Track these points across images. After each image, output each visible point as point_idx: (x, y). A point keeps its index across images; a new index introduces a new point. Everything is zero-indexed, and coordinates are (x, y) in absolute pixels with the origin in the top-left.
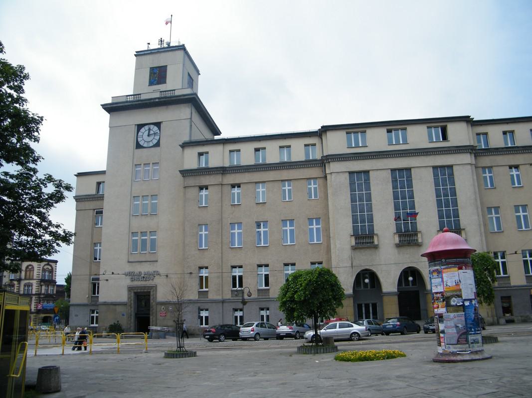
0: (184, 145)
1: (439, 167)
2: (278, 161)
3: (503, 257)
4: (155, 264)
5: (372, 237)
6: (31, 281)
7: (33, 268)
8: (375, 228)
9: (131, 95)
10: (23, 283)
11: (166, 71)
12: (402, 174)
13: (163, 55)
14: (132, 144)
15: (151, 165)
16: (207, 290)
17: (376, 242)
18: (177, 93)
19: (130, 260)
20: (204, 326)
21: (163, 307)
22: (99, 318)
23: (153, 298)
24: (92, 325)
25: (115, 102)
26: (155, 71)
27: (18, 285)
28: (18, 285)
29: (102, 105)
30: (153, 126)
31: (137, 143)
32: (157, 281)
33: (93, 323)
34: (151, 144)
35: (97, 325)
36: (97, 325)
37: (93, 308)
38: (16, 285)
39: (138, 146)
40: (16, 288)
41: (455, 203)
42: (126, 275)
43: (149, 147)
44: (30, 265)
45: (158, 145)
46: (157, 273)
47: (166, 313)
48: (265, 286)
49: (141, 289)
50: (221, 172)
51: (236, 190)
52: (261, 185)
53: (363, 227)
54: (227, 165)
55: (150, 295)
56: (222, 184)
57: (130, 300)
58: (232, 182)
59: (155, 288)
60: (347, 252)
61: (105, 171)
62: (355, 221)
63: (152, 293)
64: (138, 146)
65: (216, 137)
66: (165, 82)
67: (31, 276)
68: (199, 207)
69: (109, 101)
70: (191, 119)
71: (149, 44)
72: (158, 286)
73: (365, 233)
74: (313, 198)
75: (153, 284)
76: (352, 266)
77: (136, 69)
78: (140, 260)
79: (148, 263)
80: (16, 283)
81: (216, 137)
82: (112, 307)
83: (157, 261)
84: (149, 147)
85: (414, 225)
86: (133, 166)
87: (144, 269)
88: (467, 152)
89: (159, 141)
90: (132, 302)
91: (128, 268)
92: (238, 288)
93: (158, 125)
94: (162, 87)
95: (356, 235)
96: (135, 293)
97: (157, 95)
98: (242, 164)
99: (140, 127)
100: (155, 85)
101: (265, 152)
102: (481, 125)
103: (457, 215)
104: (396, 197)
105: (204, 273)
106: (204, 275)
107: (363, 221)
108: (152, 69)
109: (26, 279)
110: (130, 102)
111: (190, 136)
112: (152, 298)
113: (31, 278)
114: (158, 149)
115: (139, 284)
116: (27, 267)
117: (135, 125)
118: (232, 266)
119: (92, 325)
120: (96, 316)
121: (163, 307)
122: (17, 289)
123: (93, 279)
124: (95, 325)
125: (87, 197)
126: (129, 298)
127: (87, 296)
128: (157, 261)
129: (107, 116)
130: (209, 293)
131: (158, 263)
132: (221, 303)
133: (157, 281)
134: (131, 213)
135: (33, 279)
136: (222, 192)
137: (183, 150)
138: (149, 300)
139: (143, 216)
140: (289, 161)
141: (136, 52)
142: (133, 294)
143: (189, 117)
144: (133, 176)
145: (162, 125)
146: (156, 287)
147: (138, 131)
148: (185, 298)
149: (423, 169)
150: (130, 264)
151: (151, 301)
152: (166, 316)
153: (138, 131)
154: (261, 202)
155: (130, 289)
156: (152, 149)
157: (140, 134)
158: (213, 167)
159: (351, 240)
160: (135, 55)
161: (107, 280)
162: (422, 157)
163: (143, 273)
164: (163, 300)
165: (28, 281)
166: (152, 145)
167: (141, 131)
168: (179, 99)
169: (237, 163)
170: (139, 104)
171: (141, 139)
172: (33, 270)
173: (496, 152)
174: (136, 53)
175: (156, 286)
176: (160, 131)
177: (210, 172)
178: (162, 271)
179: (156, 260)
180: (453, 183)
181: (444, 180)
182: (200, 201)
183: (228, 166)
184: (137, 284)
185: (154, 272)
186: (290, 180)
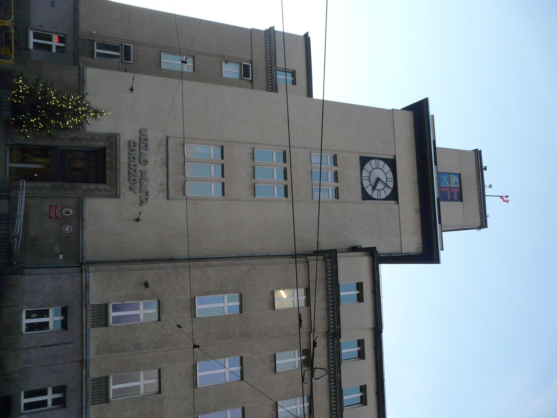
1: (106, 321)
2: (341, 282)
4: (163, 195)
15: (336, 185)
19: (170, 141)
20: (25, 321)
21: (71, 212)
24: (31, 34)
30: (392, 187)
33: (36, 36)
35: (31, 46)
36: (31, 46)
37: (69, 40)
42: (142, 133)
43: (362, 180)
45: (366, 197)
47: (57, 217)
48: (27, 324)
50: (332, 330)
57: (88, 137)
63: (101, 186)
64: (364, 160)
78: (170, 162)
79: (165, 180)
83: (168, 198)
84: (362, 180)
86: (335, 150)
88: (329, 327)
90: (84, 143)
93: (394, 196)
96: (103, 150)
98: (338, 258)
99: (392, 163)
112: (92, 186)
117: (395, 156)
119: (31, 34)
120: (51, 46)
121: (71, 212)
123: (127, 49)
124: (32, 41)
126: (93, 136)
127: (94, 33)
128: (168, 198)
132: (80, 359)
138: (86, 180)
139: (252, 169)
140: (343, 357)
142: (100, 144)
145: (393, 202)
146: (116, 196)
147: (385, 160)
148: (91, 275)
151: (85, 186)
152: (51, 217)
153: (385, 160)
157: (381, 163)
161: (132, 90)
163: (146, 168)
164: (86, 212)
166: (365, 186)
167: (386, 165)
169: (344, 353)
173: (332, 291)
175: (119, 197)
177: (335, 396)
178: (147, 209)
179: (171, 196)
184: (122, 155)
185: (147, 193)
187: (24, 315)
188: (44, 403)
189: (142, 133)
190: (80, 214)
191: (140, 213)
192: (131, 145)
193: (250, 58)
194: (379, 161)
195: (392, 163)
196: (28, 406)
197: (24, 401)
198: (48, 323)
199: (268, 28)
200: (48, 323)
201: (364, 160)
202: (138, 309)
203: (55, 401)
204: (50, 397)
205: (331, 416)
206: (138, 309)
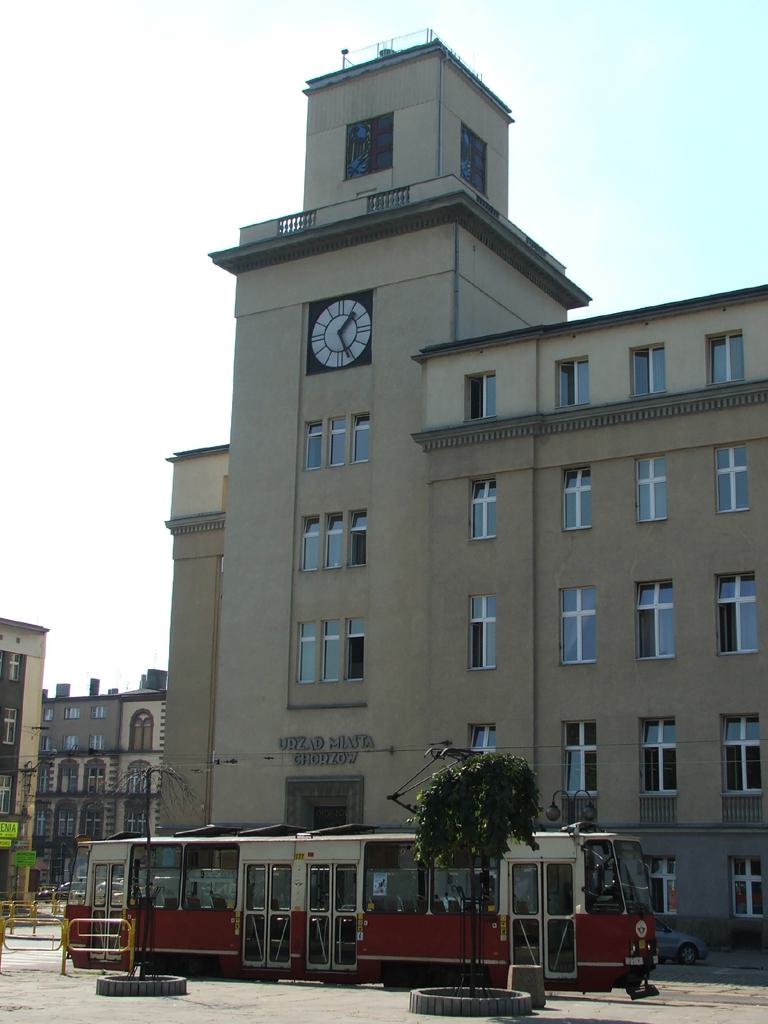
0: (427, 355)
3: (591, 739)
6: (145, 758)
7: (151, 719)
9: (296, 216)
10: (126, 761)
11: (390, 130)
14: (296, 362)
16: (755, 791)
18: (415, 196)
19: (296, 702)
22: (763, 887)
25: (251, 240)
26: (362, 133)
27: (113, 769)
28: (113, 769)
29: (211, 255)
30: (353, 302)
31: (311, 354)
38: (108, 769)
39: (314, 366)
40: (108, 776)
43: (343, 368)
44: (143, 711)
45: (365, 358)
46: (368, 742)
51: (579, 488)
54: (549, 404)
55: (345, 808)
58: (566, 461)
61: (227, 446)
65: (574, 315)
66: (389, 165)
67: (146, 741)
68: (564, 531)
69: (232, 241)
70: (456, 271)
71: (345, 52)
72: (366, 780)
74: (734, 507)
75: (354, 773)
77: (308, 135)
80: (107, 760)
81: (574, 315)
87: (328, 727)
89: (369, 345)
91: (293, 726)
93: (365, 298)
94: (380, 181)
97: (360, 209)
98: (594, 402)
99: (316, 308)
100: (364, 174)
101: (742, 343)
105: (660, 741)
106: (744, 743)
108: (352, 129)
109: (132, 750)
110: (290, 236)
113: (146, 747)
114: (365, 370)
116: (135, 717)
117: (304, 304)
118: (723, 716)
122: (111, 779)
125: (201, 520)
128: (364, 705)
129: (228, 281)
130: (763, 799)
133: (366, 764)
135: (150, 751)
136: (534, 492)
137: (424, 369)
141: (309, 82)
143: (450, 265)
154: (652, 517)
155: (293, 787)
156: (352, 371)
157: (318, 329)
163: (327, 740)
165: (136, 758)
170: (310, 242)
171: (321, 344)
172: (152, 726)
174: (307, 87)
182: (473, 526)
183: (552, 411)
186: (743, 443)
187: (744, 916)
188: (756, 886)
189: (286, 743)
190: (33, 818)
191: (233, 761)
192: (299, 760)
193: (215, 558)
194: (313, 335)
195: (316, 308)
196: (757, 909)
197: (750, 913)
198: (753, 883)
199: (169, 531)
200: (753, 883)
201: (314, 366)
202: (586, 743)
203: (756, 870)
204: (749, 878)
205: (765, 401)
206: (586, 743)
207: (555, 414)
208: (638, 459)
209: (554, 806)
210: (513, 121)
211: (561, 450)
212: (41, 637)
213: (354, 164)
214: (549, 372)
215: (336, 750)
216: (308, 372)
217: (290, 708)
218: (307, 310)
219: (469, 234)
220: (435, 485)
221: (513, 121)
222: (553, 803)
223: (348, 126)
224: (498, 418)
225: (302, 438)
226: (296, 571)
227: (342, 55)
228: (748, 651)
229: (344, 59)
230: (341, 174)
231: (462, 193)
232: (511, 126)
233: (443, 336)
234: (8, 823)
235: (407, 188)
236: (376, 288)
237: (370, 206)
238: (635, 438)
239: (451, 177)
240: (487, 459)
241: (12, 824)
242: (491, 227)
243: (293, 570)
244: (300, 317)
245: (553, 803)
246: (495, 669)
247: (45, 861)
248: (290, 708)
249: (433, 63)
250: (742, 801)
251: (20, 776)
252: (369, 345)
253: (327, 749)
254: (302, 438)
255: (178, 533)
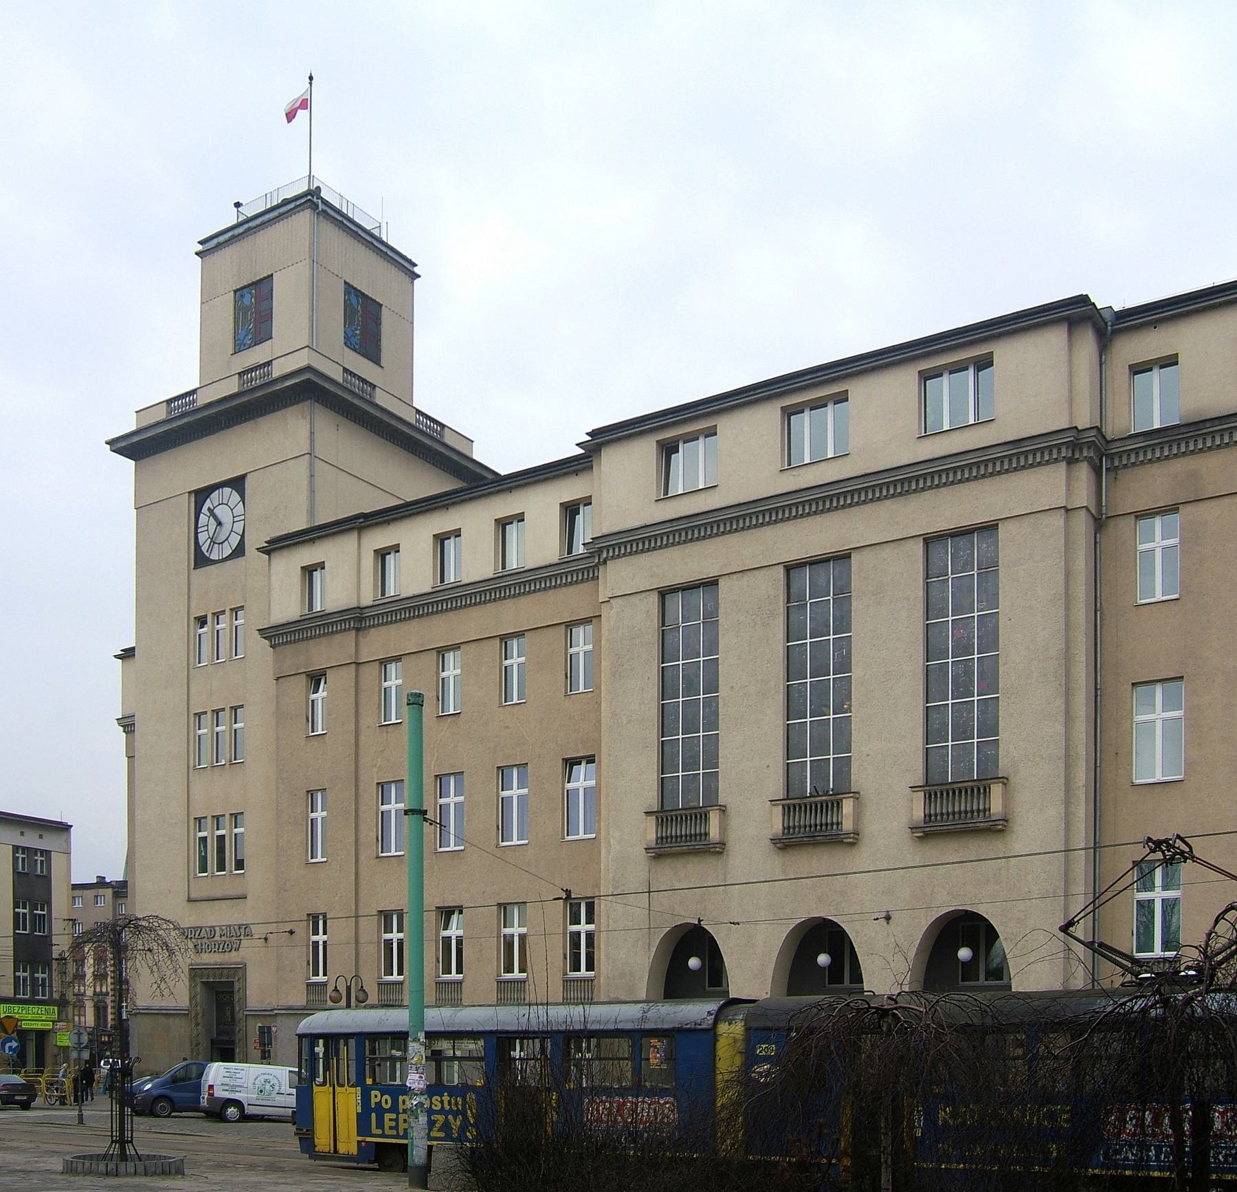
5: (705, 817)
8: (722, 785)
12: (821, 581)
13: (262, 237)
14: (184, 555)
17: (714, 833)
18: (277, 371)
19: (194, 895)
23: (240, 999)
32: (249, 952)
34: (227, 552)
39: (201, 560)
41: (990, 681)
49: (221, 976)
52: (1158, 522)
53: (962, 754)
54: (367, 598)
56: (1067, 510)
59: (240, 970)
60: (638, 870)
61: (133, 649)
62: (665, 762)
63: (237, 986)
73: (695, 804)
76: (357, 917)
82: (162, 1020)
85: (989, 754)
87: (219, 916)
89: (243, 536)
92: (583, 972)
93: (237, 484)
95: (664, 815)
99: (201, 495)
102: (1155, 324)
103: (990, 727)
104: (792, 668)
106: (516, 930)
107: (962, 731)
111: (311, 512)
114: (239, 561)
115: (212, 961)
117: (190, 492)
131: (250, 902)
133: (249, 952)
134: (191, 765)
141: (200, 243)
144: (192, 653)
149: (887, 551)
150: (193, 904)
158: (283, 621)
159: (1005, 806)
160: (197, 254)
162: (888, 503)
168: (275, 393)
174: (200, 248)
176: (243, 500)
180: (992, 599)
181: (963, 588)
194: (199, 526)
207: (373, 606)
208: (441, 651)
209: (336, 989)
210: (419, 276)
211: (378, 642)
212: (64, 836)
213: (242, 334)
214: (368, 561)
215: (224, 938)
216: (195, 565)
217: (189, 900)
218: (193, 499)
219: (290, 409)
220: (280, 680)
221: (419, 276)
222: (336, 987)
223: (235, 292)
224: (327, 612)
225: (192, 635)
226: (191, 770)
227: (236, 209)
228: (522, 842)
229: (238, 211)
230: (230, 348)
231: (309, 369)
232: (416, 281)
233: (299, 523)
234: (47, 1007)
235: (269, 363)
236: (246, 474)
237: (241, 384)
238: (438, 630)
239: (307, 349)
240: (322, 653)
241: (52, 1008)
242: (353, 403)
243: (188, 767)
244: (186, 505)
245: (336, 987)
246: (326, 862)
247: (1203, 1097)
248: (189, 900)
249: (305, 218)
250: (503, 984)
251: (54, 963)
252: (243, 536)
253: (217, 938)
254: (192, 635)
255: (128, 731)
